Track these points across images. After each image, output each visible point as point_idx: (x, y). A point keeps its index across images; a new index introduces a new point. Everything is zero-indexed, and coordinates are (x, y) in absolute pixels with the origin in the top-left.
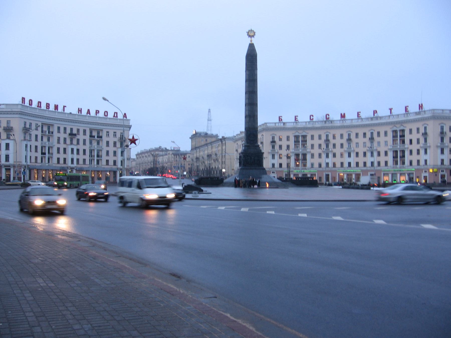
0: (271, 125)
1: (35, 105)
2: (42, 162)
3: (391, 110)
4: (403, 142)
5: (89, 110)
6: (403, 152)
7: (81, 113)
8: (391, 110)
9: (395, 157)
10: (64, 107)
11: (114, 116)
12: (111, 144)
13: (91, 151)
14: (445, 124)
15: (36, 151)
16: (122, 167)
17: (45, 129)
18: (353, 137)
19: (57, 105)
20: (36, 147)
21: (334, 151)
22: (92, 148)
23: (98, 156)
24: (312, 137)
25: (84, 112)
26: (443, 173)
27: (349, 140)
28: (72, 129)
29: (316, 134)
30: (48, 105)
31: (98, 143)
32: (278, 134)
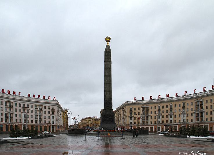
0: (130, 102)
3: (195, 90)
4: (202, 108)
5: (34, 95)
6: (202, 113)
7: (30, 96)
8: (195, 90)
9: (197, 117)
10: (19, 93)
12: (47, 113)
13: (6, 114)
17: (8, 104)
18: (173, 107)
19: (15, 92)
21: (163, 114)
22: (36, 115)
23: (40, 118)
24: (151, 108)
25: (32, 96)
27: (171, 108)
28: (24, 105)
29: (153, 106)
30: (9, 92)
32: (134, 107)
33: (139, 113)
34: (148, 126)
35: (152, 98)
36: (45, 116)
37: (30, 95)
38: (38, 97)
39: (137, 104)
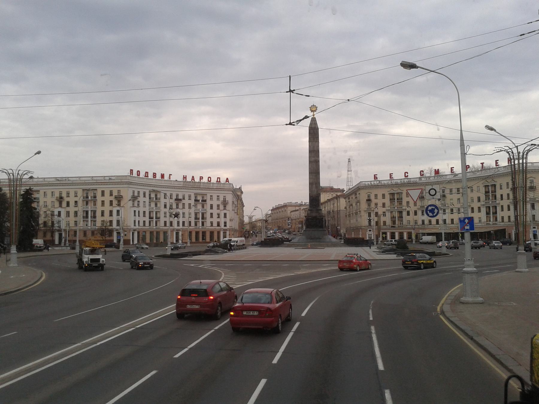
1: (142, 175)
2: (150, 225)
5: (193, 177)
9: (488, 213)
10: (170, 175)
11: (217, 181)
12: (215, 207)
14: (535, 178)
15: (144, 216)
16: (118, 227)
17: (153, 196)
20: (144, 212)
22: (196, 211)
23: (203, 218)
26: (534, 229)
28: (177, 195)
30: (155, 175)
31: (156, 205)
32: (374, 192)
33: (384, 205)
34: (402, 229)
35: (408, 176)
36: (212, 214)
37: (186, 178)
38: (200, 179)
39: (380, 186)
